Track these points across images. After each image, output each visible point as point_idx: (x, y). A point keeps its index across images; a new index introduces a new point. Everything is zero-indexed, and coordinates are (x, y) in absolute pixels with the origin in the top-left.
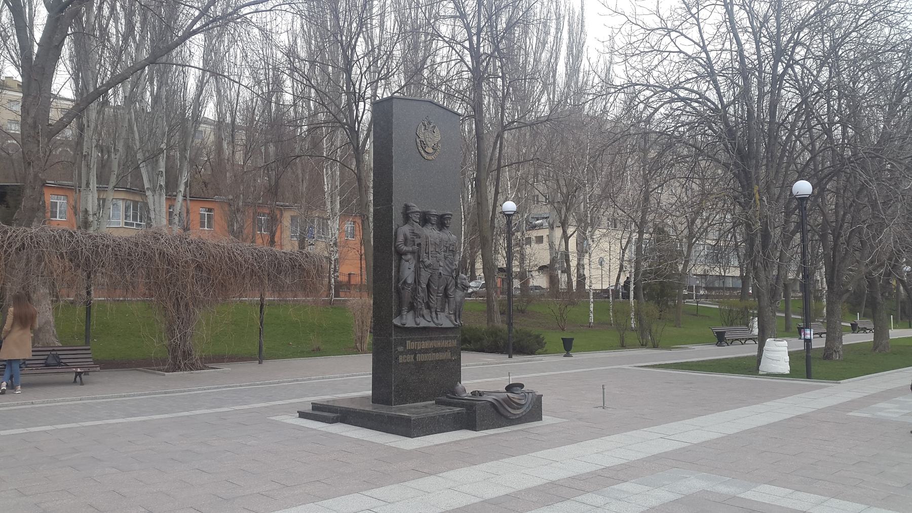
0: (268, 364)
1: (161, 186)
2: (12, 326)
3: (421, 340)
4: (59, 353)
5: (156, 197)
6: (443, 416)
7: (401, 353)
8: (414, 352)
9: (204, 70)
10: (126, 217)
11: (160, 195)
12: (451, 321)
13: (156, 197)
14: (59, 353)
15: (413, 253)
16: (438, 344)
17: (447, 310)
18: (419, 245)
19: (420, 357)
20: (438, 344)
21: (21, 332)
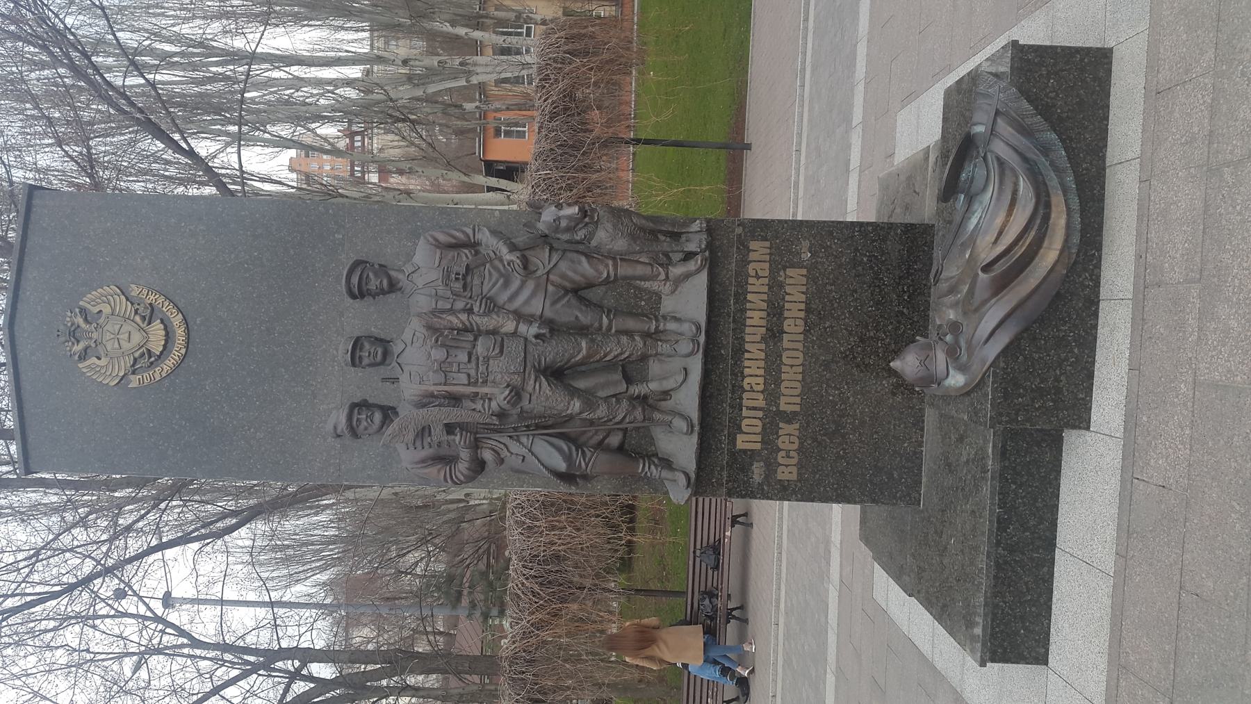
0: (754, 132)
1: (461, 64)
2: (651, 658)
3: (738, 389)
4: (698, 546)
5: (479, 70)
6: (1002, 524)
7: (771, 467)
8: (773, 419)
9: (267, 24)
10: (520, 34)
11: (475, 65)
12: (688, 276)
13: (479, 70)
14: (698, 546)
15: (476, 445)
16: (756, 319)
17: (654, 286)
18: (450, 428)
19: (789, 401)
20: (756, 319)
21: (662, 646)
